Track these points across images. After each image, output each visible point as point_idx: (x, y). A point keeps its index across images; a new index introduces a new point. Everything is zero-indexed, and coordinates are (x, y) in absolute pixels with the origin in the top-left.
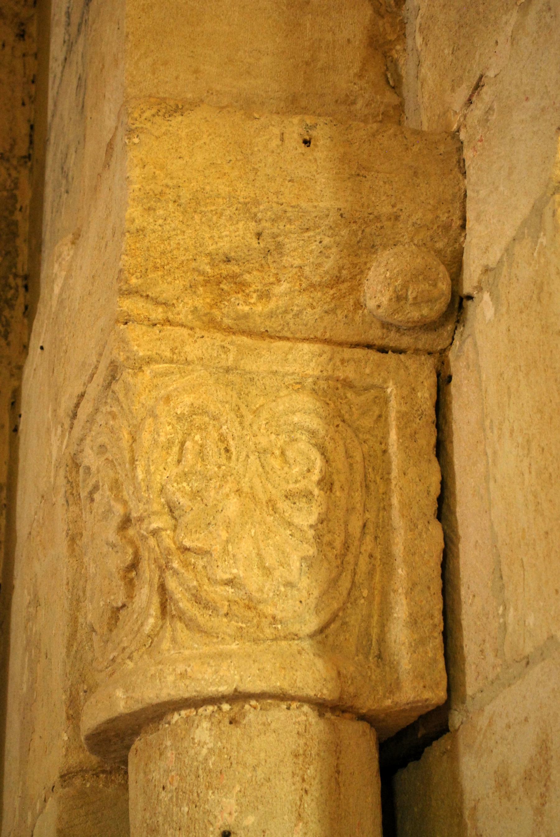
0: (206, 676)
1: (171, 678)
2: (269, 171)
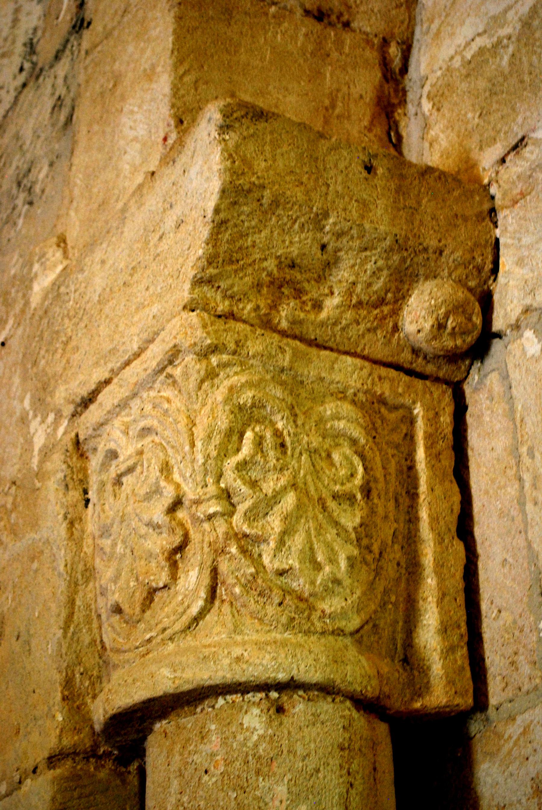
0: (265, 662)
1: (227, 661)
2: (340, 188)
